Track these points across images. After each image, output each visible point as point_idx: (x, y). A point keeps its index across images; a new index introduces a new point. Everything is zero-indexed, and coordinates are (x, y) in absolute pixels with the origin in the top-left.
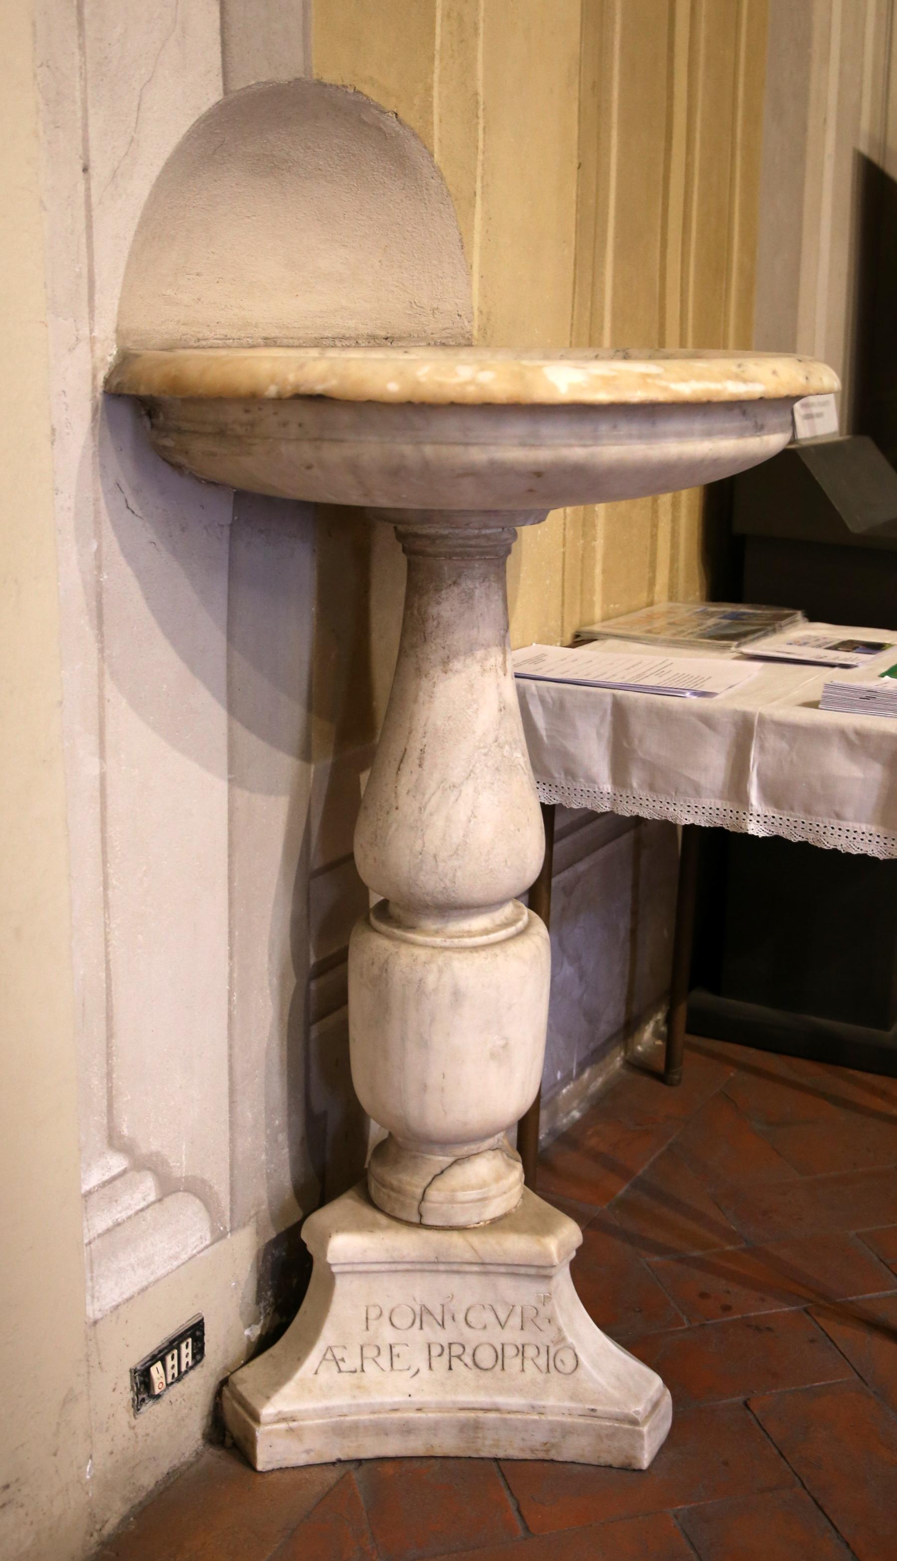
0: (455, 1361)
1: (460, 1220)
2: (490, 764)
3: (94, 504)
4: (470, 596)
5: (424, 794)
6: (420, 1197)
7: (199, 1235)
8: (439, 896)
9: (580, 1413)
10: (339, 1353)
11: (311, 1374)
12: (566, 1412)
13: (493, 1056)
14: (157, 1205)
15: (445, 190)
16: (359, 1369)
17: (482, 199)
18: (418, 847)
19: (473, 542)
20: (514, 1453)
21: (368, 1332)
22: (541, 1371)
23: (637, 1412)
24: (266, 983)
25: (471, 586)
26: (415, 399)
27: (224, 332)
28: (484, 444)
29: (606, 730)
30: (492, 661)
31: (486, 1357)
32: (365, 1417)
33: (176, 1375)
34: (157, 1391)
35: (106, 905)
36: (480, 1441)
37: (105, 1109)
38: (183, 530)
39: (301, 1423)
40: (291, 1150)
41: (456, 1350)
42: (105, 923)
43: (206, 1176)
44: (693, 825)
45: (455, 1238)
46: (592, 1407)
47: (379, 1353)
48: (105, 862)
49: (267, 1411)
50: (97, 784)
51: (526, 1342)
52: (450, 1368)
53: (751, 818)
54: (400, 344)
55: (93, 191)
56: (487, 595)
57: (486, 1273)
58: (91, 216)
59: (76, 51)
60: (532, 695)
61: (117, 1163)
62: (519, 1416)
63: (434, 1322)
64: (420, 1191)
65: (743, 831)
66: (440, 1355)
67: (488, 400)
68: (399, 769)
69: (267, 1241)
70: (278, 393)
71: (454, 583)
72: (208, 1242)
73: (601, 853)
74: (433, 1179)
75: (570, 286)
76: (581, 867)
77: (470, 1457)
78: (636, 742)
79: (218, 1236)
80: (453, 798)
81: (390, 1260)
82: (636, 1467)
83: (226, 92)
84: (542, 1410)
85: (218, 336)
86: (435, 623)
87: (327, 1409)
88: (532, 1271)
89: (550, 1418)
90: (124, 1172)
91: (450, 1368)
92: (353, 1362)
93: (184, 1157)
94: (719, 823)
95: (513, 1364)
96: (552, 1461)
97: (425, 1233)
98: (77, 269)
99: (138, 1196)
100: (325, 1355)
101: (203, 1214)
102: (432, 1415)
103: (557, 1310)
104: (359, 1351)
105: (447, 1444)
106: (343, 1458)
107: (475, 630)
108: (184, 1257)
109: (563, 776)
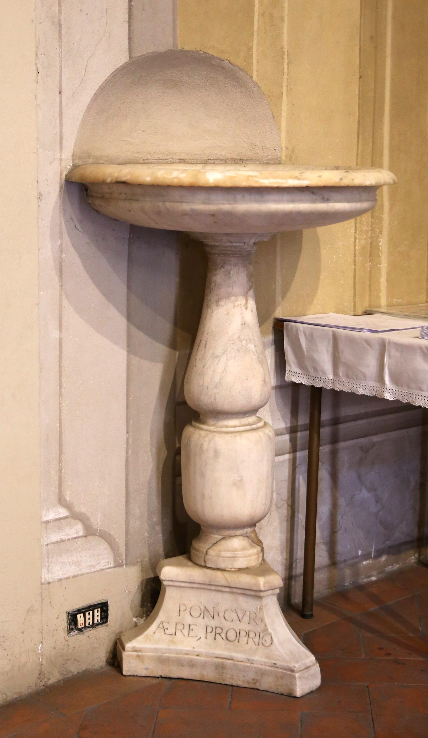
0: (217, 636)
1: (222, 565)
2: (235, 348)
3: (60, 225)
4: (229, 273)
5: (205, 360)
6: (205, 553)
7: (107, 560)
8: (210, 406)
9: (269, 665)
10: (166, 625)
11: (152, 633)
12: (263, 664)
13: (234, 484)
14: (84, 538)
15: (261, 93)
16: (174, 634)
17: (287, 96)
18: (201, 383)
19: (229, 249)
20: (240, 683)
21: (180, 617)
22: (255, 644)
23: (295, 667)
24: (149, 449)
25: (229, 268)
26: (155, 184)
27: (158, 156)
28: (188, 202)
29: (330, 349)
30: (238, 303)
31: (232, 635)
32: (173, 655)
33: (91, 624)
34: (80, 627)
35: (61, 394)
36: (224, 675)
37: (57, 485)
38: (103, 239)
39: (143, 653)
40: (163, 536)
41: (219, 630)
42: (60, 403)
43: (112, 533)
44: (364, 395)
45: (219, 574)
46: (275, 662)
47: (184, 628)
48: (60, 376)
49: (129, 646)
50: (58, 342)
51: (251, 630)
52: (215, 639)
53: (386, 390)
54: (247, 163)
55: (63, 101)
56: (237, 273)
57: (232, 593)
58: (62, 111)
59: (58, 48)
60: (301, 331)
61: (63, 512)
62: (242, 663)
63: (210, 616)
64: (205, 550)
65: (383, 397)
66: (211, 632)
67: (181, 185)
68: (198, 349)
69: (148, 577)
70: (111, 181)
71: (222, 267)
72: (112, 565)
73: (394, 434)
74: (212, 545)
75: (356, 137)
76: (375, 439)
77: (221, 684)
78: (341, 353)
79: (118, 565)
80: (216, 362)
81: (189, 581)
82: (294, 695)
83: (130, 58)
84: (252, 662)
85: (155, 158)
86: (214, 284)
87: (155, 649)
88: (252, 593)
89: (255, 665)
90: (66, 518)
91: (215, 639)
92: (171, 630)
93: (99, 520)
94: (375, 394)
95: (244, 640)
96: (257, 689)
97: (206, 570)
98: (55, 132)
99: (73, 531)
100: (159, 625)
101: (109, 550)
102: (202, 658)
103: (265, 615)
104: (175, 625)
105: (210, 675)
106: (163, 675)
107: (231, 288)
108: (97, 568)
109: (313, 371)
